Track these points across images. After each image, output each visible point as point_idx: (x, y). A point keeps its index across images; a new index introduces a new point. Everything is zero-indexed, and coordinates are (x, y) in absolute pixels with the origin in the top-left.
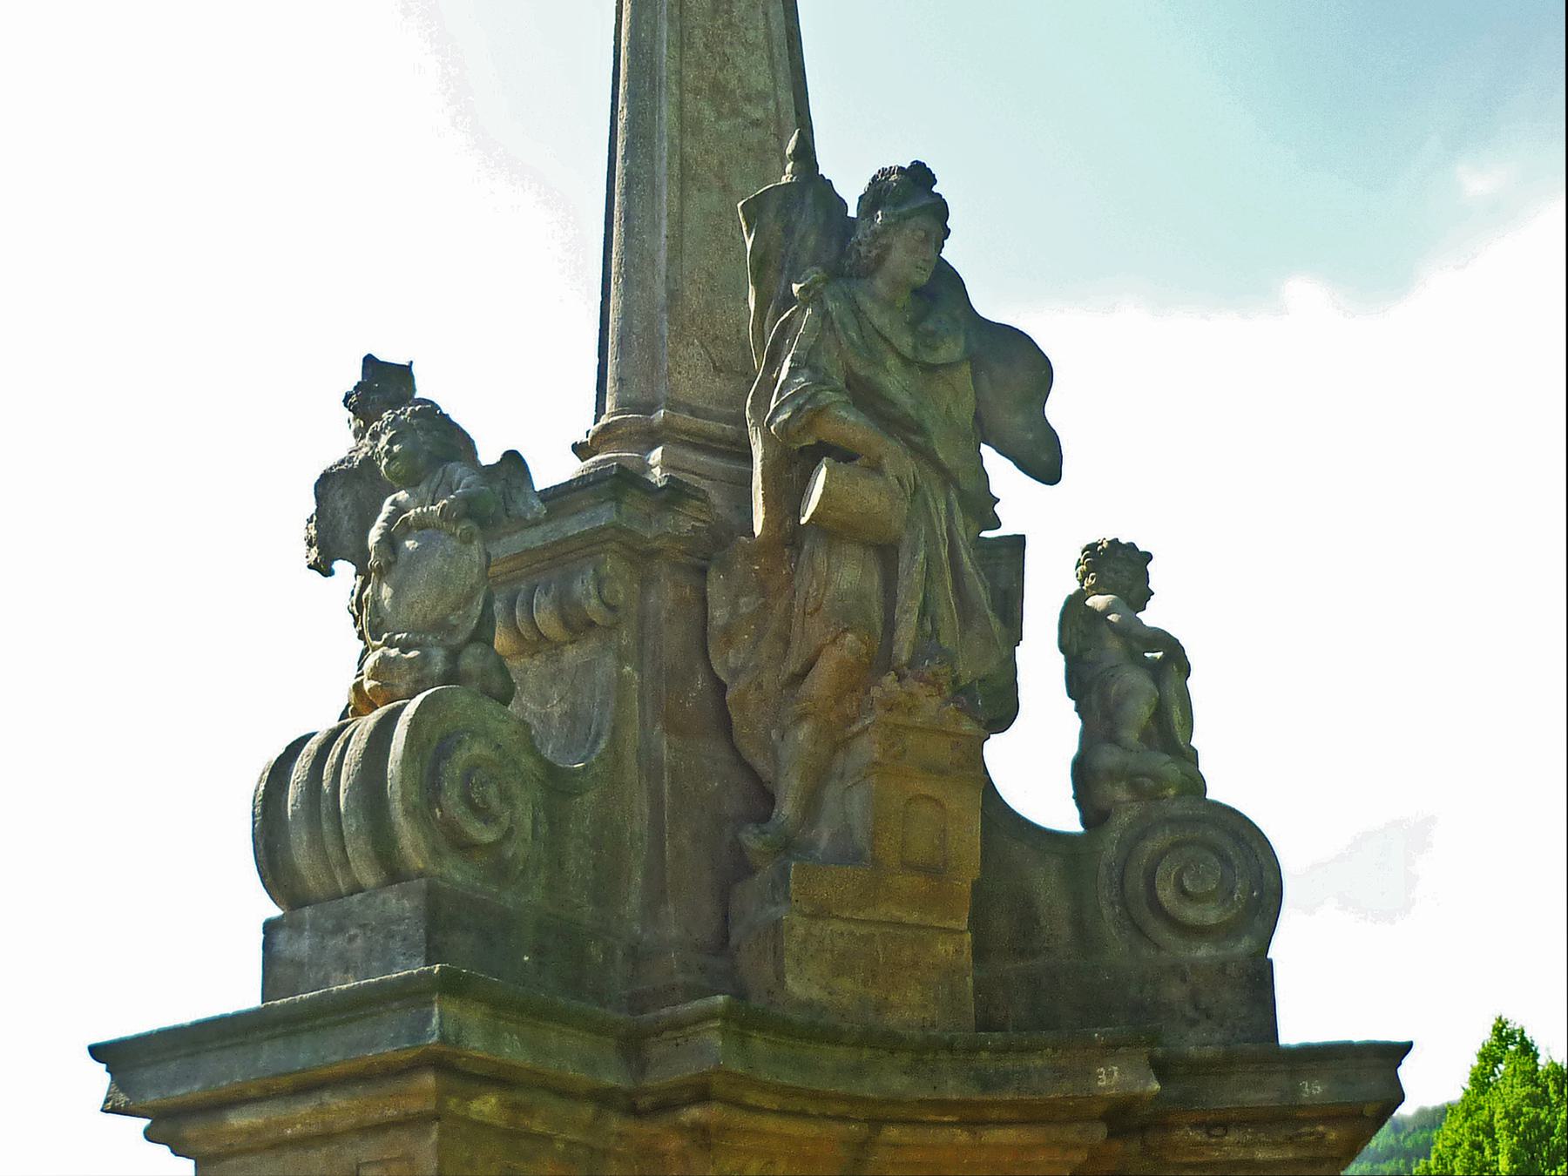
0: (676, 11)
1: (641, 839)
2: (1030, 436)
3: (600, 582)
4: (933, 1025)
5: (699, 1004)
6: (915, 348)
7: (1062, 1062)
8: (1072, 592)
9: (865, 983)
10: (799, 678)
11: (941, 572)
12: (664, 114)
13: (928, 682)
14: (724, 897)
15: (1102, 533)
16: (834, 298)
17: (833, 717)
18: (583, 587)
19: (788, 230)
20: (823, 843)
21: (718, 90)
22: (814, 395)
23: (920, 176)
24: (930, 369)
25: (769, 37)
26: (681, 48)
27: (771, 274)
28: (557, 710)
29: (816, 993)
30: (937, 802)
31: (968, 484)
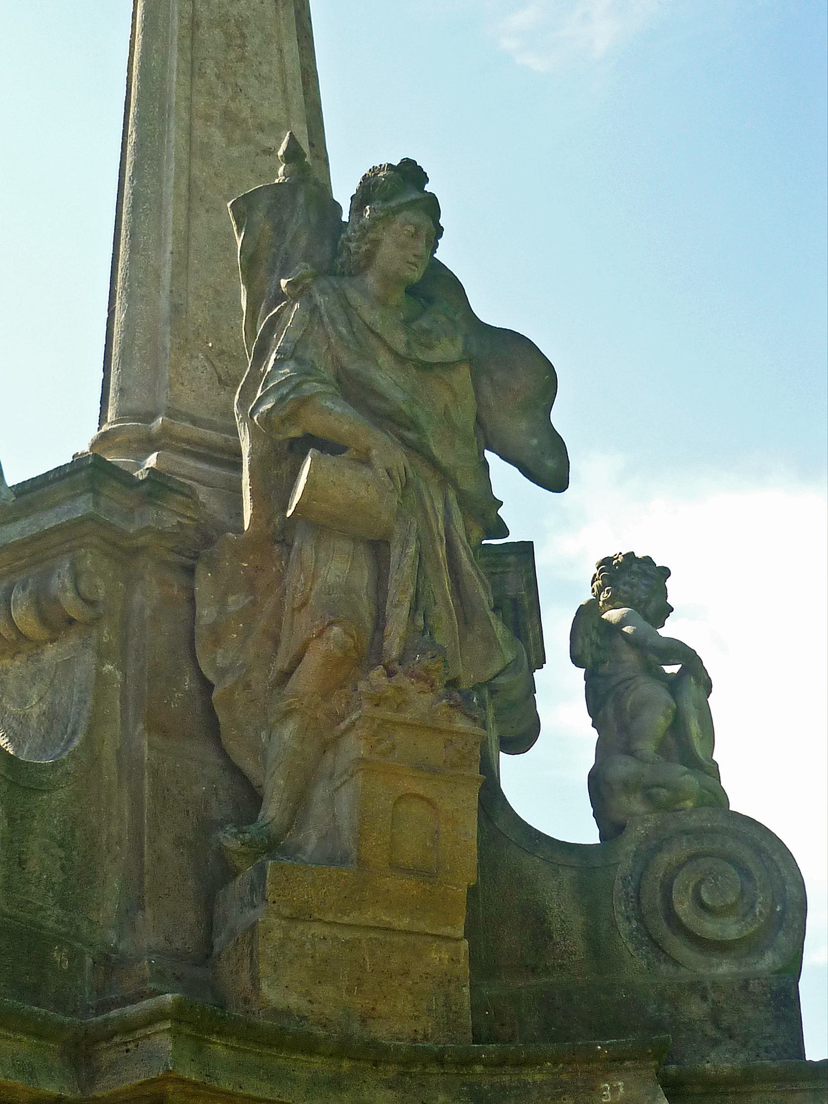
0: (187, 42)
1: (119, 843)
2: (535, 441)
3: (76, 577)
4: (425, 1037)
5: (148, 1004)
6: (408, 344)
7: (565, 1077)
8: (583, 602)
9: (349, 991)
10: (286, 676)
11: (438, 569)
12: (173, 136)
13: (419, 678)
14: (209, 900)
15: (615, 548)
16: (323, 292)
17: (320, 714)
18: (61, 583)
19: (279, 229)
20: (310, 848)
21: (230, 118)
22: (298, 385)
23: (410, 174)
24: (427, 367)
25: (283, 72)
26: (192, 76)
27: (262, 273)
28: (35, 710)
29: (294, 1001)
30: (430, 802)
31: (469, 485)
